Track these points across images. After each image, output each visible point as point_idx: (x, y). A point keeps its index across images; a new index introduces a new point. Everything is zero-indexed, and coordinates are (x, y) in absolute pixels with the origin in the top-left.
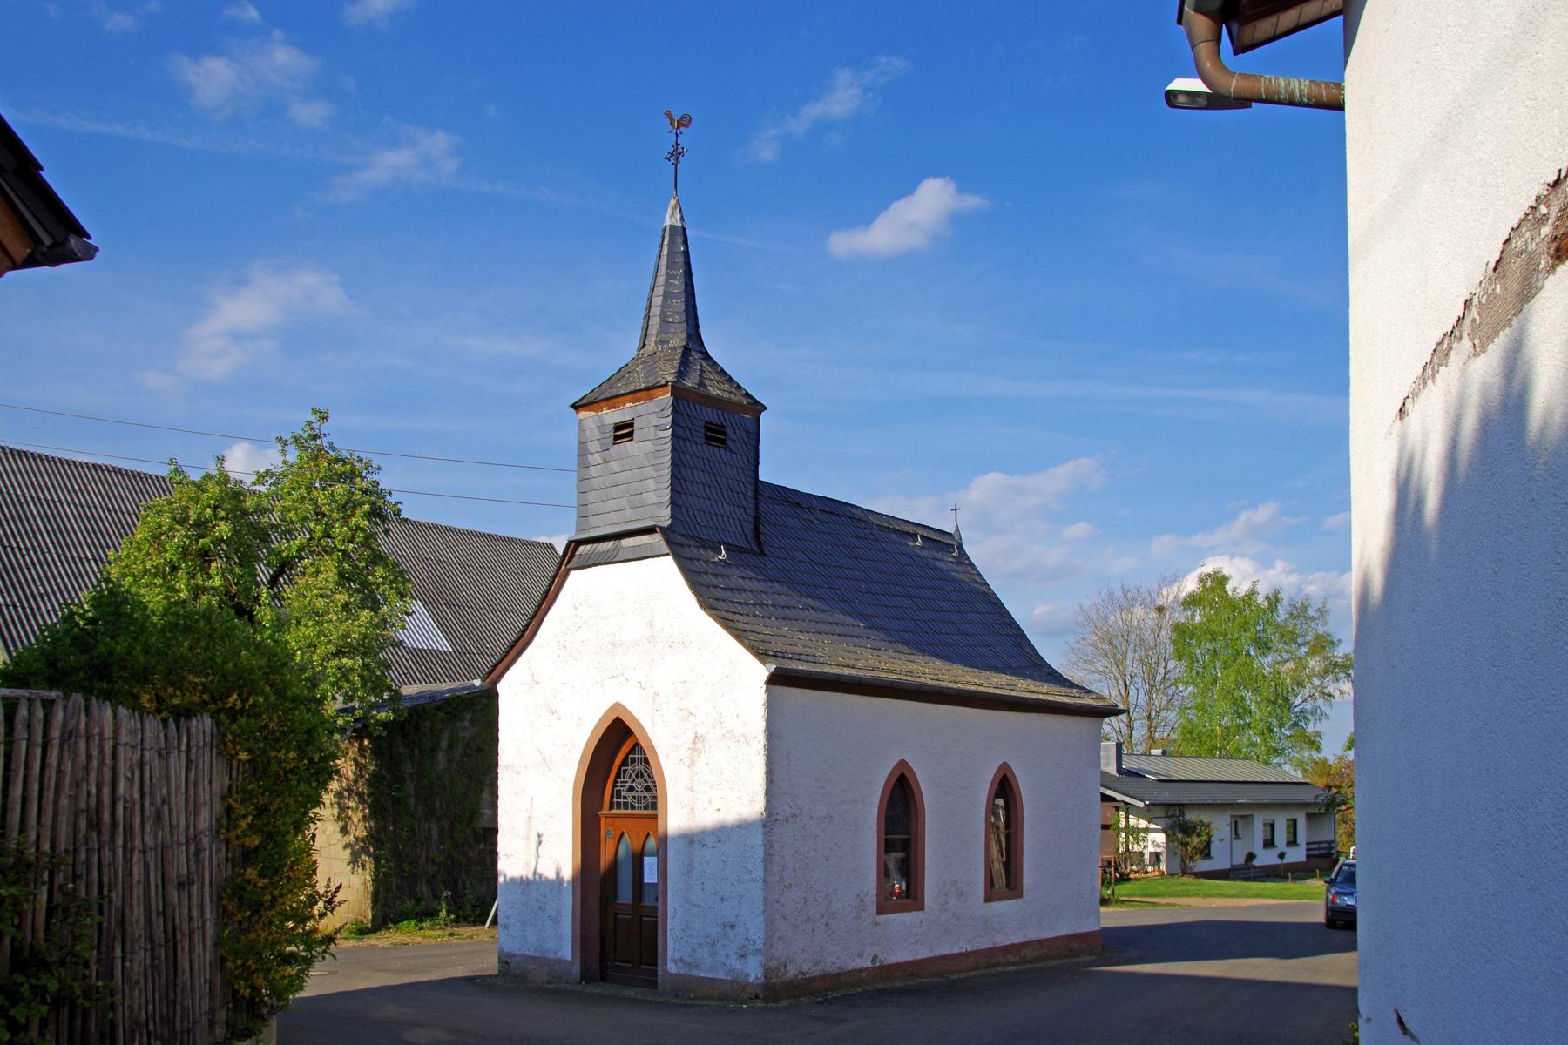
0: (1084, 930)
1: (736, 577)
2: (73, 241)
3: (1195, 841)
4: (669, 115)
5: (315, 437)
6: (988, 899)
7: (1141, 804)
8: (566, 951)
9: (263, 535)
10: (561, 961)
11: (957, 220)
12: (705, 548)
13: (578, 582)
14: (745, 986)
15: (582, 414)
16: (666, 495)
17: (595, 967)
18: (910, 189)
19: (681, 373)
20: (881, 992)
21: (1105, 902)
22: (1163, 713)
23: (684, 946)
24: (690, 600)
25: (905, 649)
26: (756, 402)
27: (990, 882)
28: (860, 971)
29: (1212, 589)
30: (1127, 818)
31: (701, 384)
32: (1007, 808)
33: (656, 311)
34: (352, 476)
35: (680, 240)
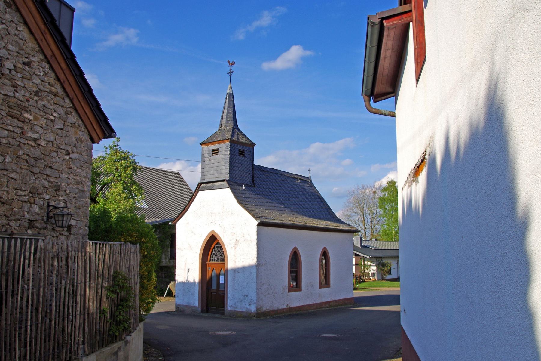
0: (349, 297)
1: (248, 194)
2: (113, 134)
3: (386, 269)
4: (229, 62)
5: (116, 146)
6: (320, 288)
7: (368, 257)
8: (197, 305)
9: (98, 175)
10: (195, 307)
11: (304, 59)
12: (239, 185)
13: (200, 193)
14: (251, 313)
15: (203, 146)
16: (228, 171)
17: (205, 308)
18: (287, 48)
19: (232, 136)
20: (290, 315)
21: (355, 289)
22: (376, 226)
23: (231, 303)
24: (235, 201)
25: (296, 214)
26: (253, 143)
27: (320, 283)
28: (283, 309)
29: (391, 186)
30: (364, 261)
31: (238, 139)
32: (325, 260)
33: (225, 117)
34: (126, 159)
35: (231, 97)
